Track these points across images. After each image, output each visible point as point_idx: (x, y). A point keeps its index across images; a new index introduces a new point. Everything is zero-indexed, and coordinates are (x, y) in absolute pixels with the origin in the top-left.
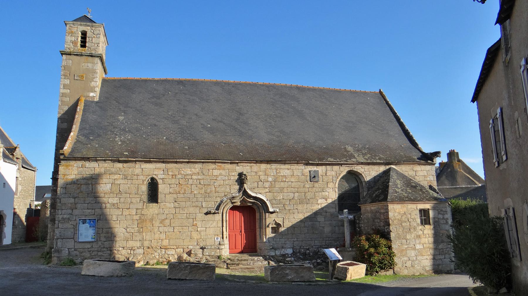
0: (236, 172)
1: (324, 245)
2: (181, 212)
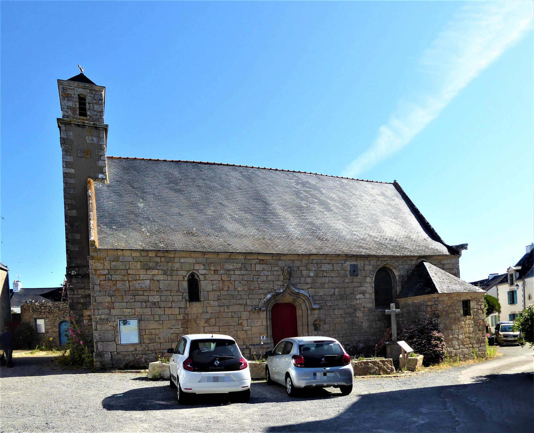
0: (278, 266)
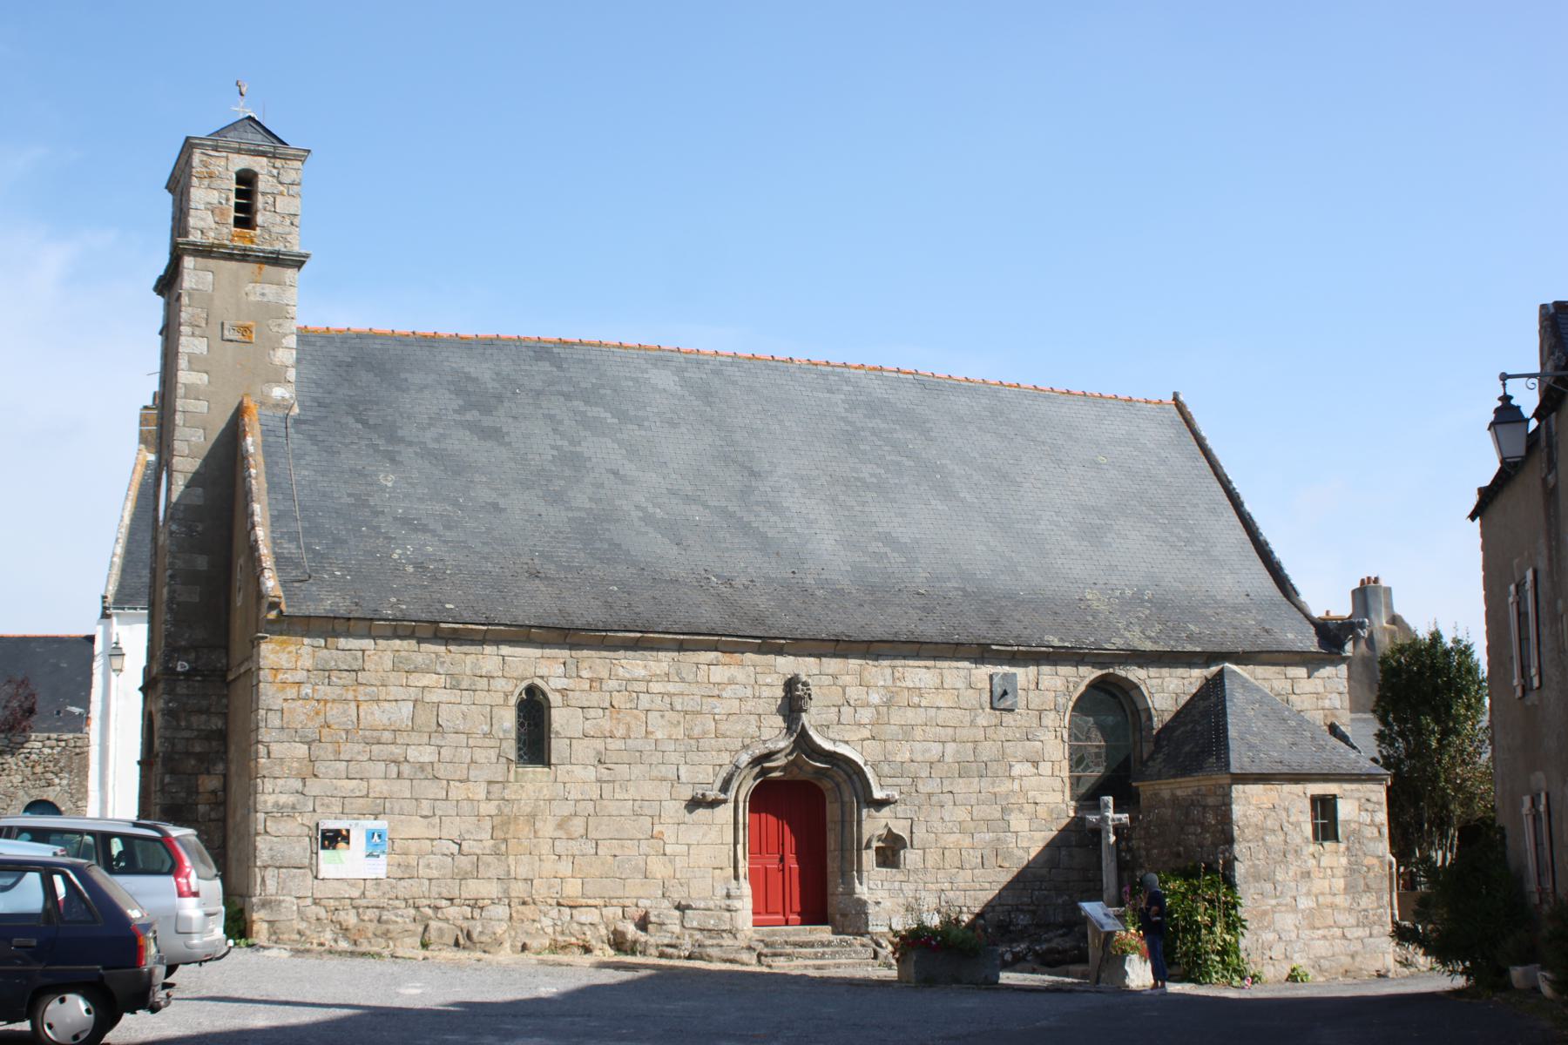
0: (776, 672)
1: (1029, 905)
2: (617, 796)
